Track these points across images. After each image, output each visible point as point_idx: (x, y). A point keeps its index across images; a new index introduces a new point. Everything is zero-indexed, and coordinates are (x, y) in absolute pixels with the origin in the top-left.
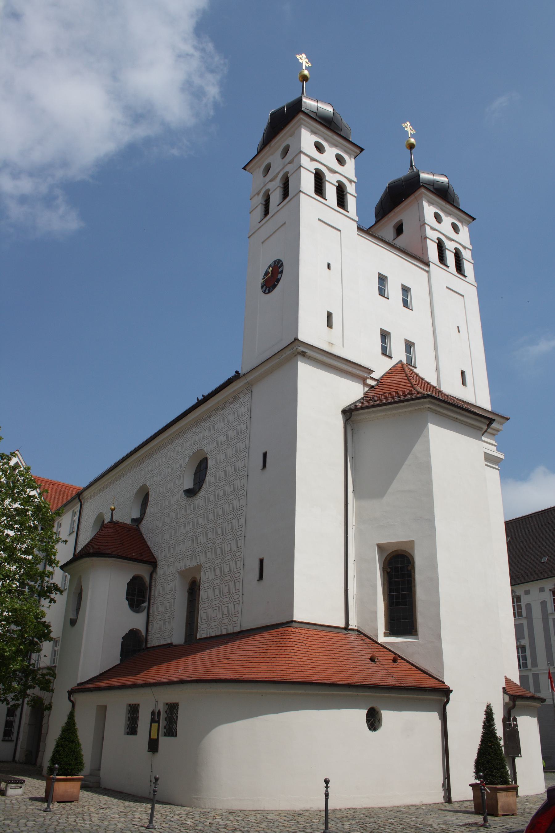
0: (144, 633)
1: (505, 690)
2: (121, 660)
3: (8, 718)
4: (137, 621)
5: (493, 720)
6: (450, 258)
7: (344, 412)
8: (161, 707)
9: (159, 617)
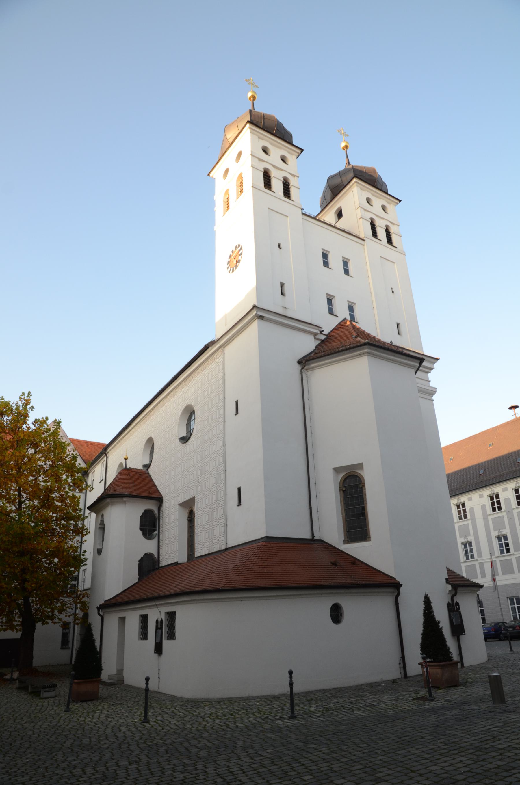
0: (156, 556)
1: (447, 581)
2: (139, 579)
3: (64, 631)
4: (150, 546)
5: (432, 607)
6: (381, 233)
7: (299, 362)
8: (163, 617)
9: (167, 542)
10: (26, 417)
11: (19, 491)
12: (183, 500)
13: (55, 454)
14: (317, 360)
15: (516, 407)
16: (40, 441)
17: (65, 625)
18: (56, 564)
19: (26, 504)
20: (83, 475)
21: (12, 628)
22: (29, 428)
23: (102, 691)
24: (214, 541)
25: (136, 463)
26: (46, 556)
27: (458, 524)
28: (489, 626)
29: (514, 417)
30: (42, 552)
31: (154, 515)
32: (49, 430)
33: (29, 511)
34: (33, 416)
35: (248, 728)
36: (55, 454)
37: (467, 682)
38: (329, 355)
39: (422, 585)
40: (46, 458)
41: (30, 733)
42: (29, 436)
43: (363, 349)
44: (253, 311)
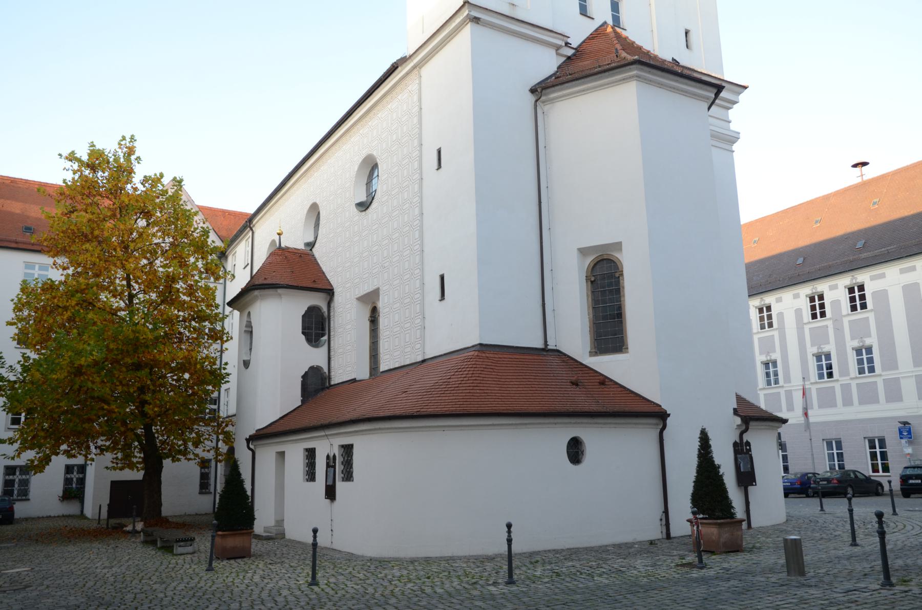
0: (326, 370)
1: (736, 412)
4: (316, 357)
5: (710, 446)
7: (533, 91)
8: (336, 451)
9: (341, 350)
10: (130, 173)
11: (128, 279)
12: (362, 293)
13: (176, 227)
14: (559, 87)
15: (864, 164)
16: (154, 208)
17: (204, 463)
18: (186, 381)
19: (139, 299)
20: (220, 258)
21: (131, 466)
22: (136, 189)
23: (256, 546)
24: (407, 350)
25: (295, 240)
26: (172, 370)
27: (758, 335)
28: (793, 477)
29: (859, 180)
30: (166, 364)
31: (322, 315)
32: (167, 191)
33: (144, 307)
34: (140, 172)
35: (450, 595)
36: (176, 227)
37: (754, 547)
38: (577, 79)
39: (700, 415)
40: (163, 233)
41: (162, 595)
42: (137, 201)
43: (631, 70)
44: (463, 10)
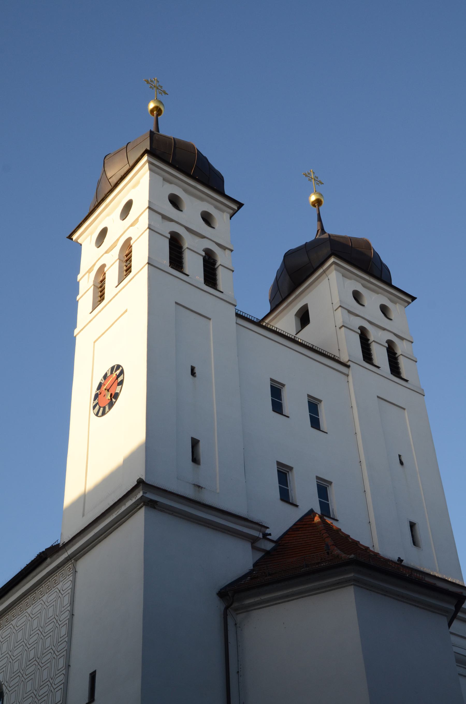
6: (380, 355)
